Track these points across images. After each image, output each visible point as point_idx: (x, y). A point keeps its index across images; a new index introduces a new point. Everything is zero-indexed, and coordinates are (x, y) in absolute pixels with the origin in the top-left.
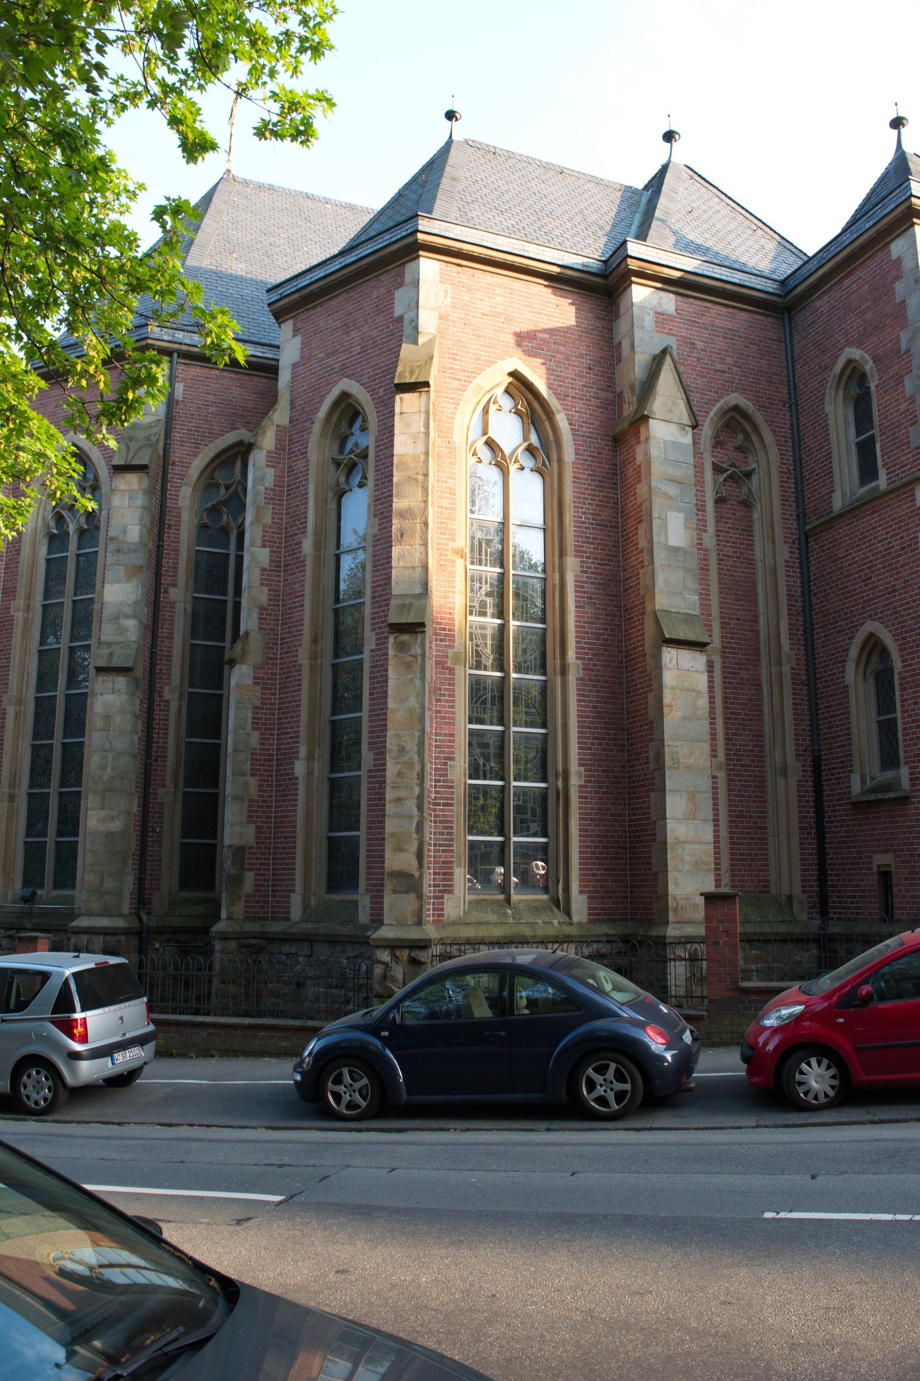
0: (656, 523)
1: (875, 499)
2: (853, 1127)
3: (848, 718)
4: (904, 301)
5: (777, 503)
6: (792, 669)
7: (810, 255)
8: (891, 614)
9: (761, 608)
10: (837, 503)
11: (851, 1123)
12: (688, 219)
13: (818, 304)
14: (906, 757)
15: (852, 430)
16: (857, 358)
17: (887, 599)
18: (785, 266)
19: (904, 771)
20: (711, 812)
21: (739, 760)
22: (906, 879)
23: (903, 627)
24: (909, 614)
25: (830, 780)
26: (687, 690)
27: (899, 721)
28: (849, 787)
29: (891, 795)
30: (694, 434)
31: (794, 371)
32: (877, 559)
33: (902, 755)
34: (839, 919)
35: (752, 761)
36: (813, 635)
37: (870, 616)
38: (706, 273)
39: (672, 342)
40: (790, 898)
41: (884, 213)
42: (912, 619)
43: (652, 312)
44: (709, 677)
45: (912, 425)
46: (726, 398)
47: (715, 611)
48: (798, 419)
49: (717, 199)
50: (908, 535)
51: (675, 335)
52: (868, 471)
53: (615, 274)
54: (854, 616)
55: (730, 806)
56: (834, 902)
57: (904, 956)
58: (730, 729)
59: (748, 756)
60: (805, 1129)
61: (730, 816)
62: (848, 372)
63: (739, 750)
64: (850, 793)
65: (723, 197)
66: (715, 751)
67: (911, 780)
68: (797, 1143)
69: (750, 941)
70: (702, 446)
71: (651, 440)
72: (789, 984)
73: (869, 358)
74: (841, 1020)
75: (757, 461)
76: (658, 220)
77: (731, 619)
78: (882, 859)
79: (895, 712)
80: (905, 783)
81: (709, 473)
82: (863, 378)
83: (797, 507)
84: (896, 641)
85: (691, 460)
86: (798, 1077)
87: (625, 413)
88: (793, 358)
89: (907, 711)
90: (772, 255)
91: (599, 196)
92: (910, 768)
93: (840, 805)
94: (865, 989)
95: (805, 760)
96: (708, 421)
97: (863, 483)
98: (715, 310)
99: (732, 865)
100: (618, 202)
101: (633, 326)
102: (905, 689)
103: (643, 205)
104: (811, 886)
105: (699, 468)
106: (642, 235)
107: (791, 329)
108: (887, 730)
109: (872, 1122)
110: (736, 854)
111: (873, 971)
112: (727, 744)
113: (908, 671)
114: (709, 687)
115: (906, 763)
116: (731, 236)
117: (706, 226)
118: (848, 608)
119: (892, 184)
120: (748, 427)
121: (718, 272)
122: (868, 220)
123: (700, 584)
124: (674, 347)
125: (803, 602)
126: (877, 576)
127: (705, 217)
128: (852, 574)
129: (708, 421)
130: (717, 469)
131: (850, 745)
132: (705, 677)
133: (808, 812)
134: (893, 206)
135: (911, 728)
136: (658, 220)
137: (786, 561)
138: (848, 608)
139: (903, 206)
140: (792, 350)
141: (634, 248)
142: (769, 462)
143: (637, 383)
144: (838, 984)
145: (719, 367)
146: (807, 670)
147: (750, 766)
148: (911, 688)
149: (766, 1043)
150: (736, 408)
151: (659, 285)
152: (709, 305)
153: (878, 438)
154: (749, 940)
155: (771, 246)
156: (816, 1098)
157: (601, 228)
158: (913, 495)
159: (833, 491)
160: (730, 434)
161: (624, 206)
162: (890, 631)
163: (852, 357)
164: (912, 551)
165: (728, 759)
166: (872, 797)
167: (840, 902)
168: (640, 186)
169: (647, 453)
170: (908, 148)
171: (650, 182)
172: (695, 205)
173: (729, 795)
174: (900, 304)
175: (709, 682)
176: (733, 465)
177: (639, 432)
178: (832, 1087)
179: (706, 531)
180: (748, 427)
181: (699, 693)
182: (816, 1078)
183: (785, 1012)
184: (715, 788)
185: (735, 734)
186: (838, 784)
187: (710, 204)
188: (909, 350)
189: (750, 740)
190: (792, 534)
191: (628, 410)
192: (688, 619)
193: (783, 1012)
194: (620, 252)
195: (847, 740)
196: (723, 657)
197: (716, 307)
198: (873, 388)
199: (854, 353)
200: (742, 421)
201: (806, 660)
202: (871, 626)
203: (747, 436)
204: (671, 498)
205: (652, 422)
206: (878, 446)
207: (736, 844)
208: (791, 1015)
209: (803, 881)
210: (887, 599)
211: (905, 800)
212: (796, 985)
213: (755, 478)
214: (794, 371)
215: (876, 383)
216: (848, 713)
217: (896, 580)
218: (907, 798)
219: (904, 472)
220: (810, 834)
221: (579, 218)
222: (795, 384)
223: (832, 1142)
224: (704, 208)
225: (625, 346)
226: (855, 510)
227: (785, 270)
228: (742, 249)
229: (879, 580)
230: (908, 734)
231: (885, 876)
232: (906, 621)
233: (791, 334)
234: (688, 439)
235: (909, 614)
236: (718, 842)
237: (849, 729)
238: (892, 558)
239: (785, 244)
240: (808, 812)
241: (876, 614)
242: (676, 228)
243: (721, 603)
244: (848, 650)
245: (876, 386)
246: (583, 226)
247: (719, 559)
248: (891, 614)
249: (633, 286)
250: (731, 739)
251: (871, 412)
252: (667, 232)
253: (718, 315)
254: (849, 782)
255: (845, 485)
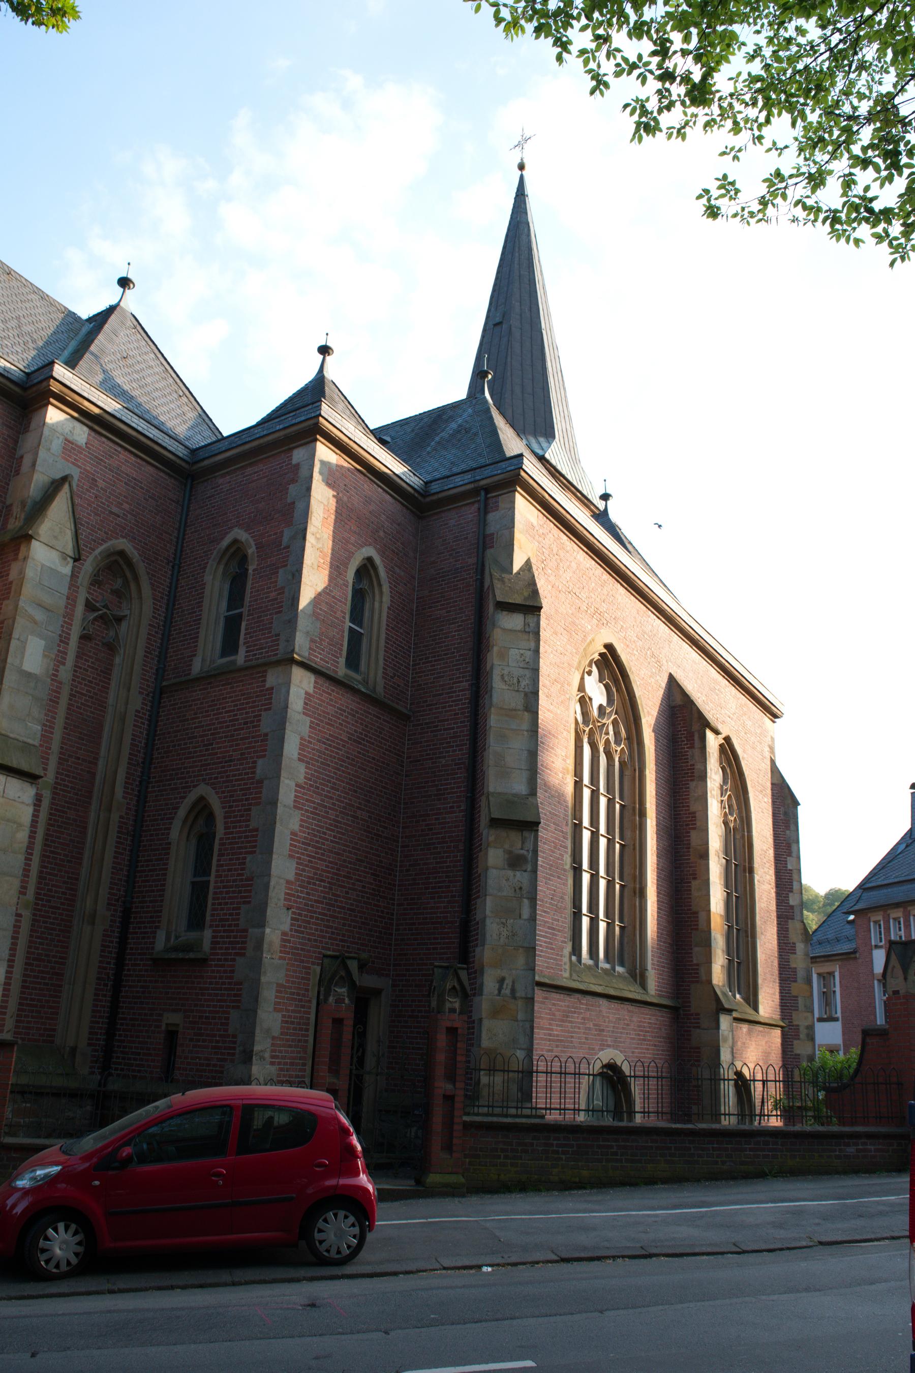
0: (14, 643)
1: (231, 672)
2: (91, 1297)
3: (165, 875)
4: (294, 503)
5: (140, 653)
6: (121, 817)
7: (225, 434)
8: (224, 782)
9: (103, 752)
10: (197, 667)
11: (89, 1293)
12: (121, 363)
13: (220, 481)
14: (212, 921)
15: (224, 604)
16: (243, 540)
17: (223, 767)
18: (199, 437)
19: (208, 934)
20: (7, 952)
21: (49, 901)
22: (191, 1040)
23: (231, 796)
24: (240, 785)
25: (136, 933)
26: (8, 820)
27: (212, 885)
28: (154, 943)
29: (191, 955)
30: (74, 567)
31: (184, 535)
32: (221, 728)
33: (208, 918)
34: (118, 1075)
35: (62, 904)
36: (147, 787)
37: (204, 780)
38: (124, 418)
39: (75, 472)
40: (74, 1050)
41: (294, 422)
42: (242, 790)
43: (61, 438)
44: (35, 810)
45: (276, 613)
46: (114, 542)
47: (55, 746)
48: (178, 580)
49: (153, 356)
50: (253, 712)
51: (79, 467)
52: (230, 645)
53: (34, 389)
54: (190, 777)
55: (30, 947)
56: (118, 1058)
57: (171, 1118)
58: (46, 867)
59: (59, 898)
60: (40, 1301)
61: (27, 958)
62: (232, 550)
63: (50, 890)
64: (153, 948)
65: (159, 356)
66: (26, 888)
67: (212, 943)
68: (25, 1317)
69: (22, 1093)
70: (80, 580)
71: (30, 560)
72: (56, 1141)
73: (253, 543)
74: (97, 1183)
75: (130, 609)
76: (92, 354)
77: (70, 756)
78: (172, 1018)
79: (210, 875)
80: (207, 946)
81: (80, 608)
82: (244, 559)
83: (158, 661)
84: (223, 808)
85: (65, 591)
86: (42, 1243)
87: (10, 526)
88: (186, 523)
89: (221, 876)
90: (190, 423)
91: (40, 311)
92: (214, 931)
93: (141, 960)
94: (126, 1151)
95: (115, 910)
96: (91, 558)
97: (223, 655)
98: (123, 455)
99: (19, 1010)
100: (58, 322)
101: (39, 445)
102: (223, 855)
103: (81, 336)
104: (98, 1039)
105: (71, 600)
106: (72, 363)
107: (190, 496)
108: (199, 891)
109: (111, 1292)
110: (26, 999)
111: (141, 1130)
112: (39, 883)
113: (229, 838)
114: (33, 821)
115: (211, 926)
116: (157, 394)
117: (136, 376)
118: (185, 768)
119: (308, 399)
120: (128, 574)
121: (135, 422)
122: (279, 423)
123: (46, 715)
124: (76, 478)
125: (145, 754)
126: (218, 743)
127: (137, 368)
128: (195, 737)
129: (91, 558)
130: (90, 606)
131: (162, 901)
132: (30, 810)
133: (109, 963)
134: (303, 418)
135: (221, 893)
136: (92, 354)
137: (137, 711)
138: (185, 768)
139: (312, 422)
140: (187, 515)
141: (60, 371)
142: (142, 612)
143: (29, 501)
144: (100, 1144)
145: (115, 510)
146: (135, 821)
147: (59, 908)
148: (228, 854)
149: (14, 1206)
150: (122, 553)
151: (76, 415)
152: (119, 449)
153: (245, 618)
154: (21, 1091)
155: (191, 415)
156: (57, 1266)
157: (34, 341)
158: (265, 676)
159: (195, 655)
160: (109, 577)
161: (63, 328)
162: (220, 798)
163: (239, 538)
164: (254, 727)
165: (36, 899)
166: (173, 956)
167: (124, 1058)
168: (84, 316)
169: (22, 573)
170: (329, 374)
171: (95, 316)
172: (131, 353)
173: (31, 936)
174: (289, 504)
175: (33, 815)
176: (106, 607)
177: (19, 549)
178: (76, 1254)
179: (64, 664)
180: (128, 574)
181: (20, 825)
182: (61, 1244)
183: (40, 1172)
184: (17, 927)
185: (50, 874)
186: (143, 938)
187: (145, 357)
188: (288, 547)
189: (64, 882)
190: (148, 686)
191: (14, 524)
192: (25, 747)
193: (38, 1173)
194: (46, 370)
195: (160, 896)
196: (54, 793)
197: (126, 453)
198: (250, 571)
199: (242, 535)
200: (125, 567)
201: (136, 811)
202: (203, 790)
203: (126, 583)
204: (35, 622)
205: (35, 544)
206: (244, 624)
207: (28, 988)
208: (46, 1176)
209: (90, 1033)
210: (223, 767)
211: (203, 962)
212: (61, 1142)
213: (124, 624)
214: (184, 535)
215: (255, 567)
216: (166, 869)
217: (234, 751)
218: (205, 960)
219: (261, 653)
220: (106, 985)
221: (14, 323)
222: (182, 547)
223: (63, 1314)
224: (139, 358)
225: (27, 461)
226: (209, 678)
227: (200, 440)
228: (165, 409)
229: (218, 748)
230: (218, 899)
231: (172, 1035)
232: (235, 791)
233: (190, 500)
234: (67, 570)
235: (240, 785)
236: (9, 984)
237: (164, 885)
238: (235, 730)
239: (204, 418)
240: (109, 963)
241: (210, 779)
242: (109, 367)
243: (63, 738)
244: (177, 808)
245: (254, 570)
246: (16, 332)
247: (71, 695)
248: (224, 782)
249: (50, 408)
250: (45, 878)
251: (244, 592)
252: (98, 368)
253: (125, 461)
254: (154, 938)
255: (206, 653)
